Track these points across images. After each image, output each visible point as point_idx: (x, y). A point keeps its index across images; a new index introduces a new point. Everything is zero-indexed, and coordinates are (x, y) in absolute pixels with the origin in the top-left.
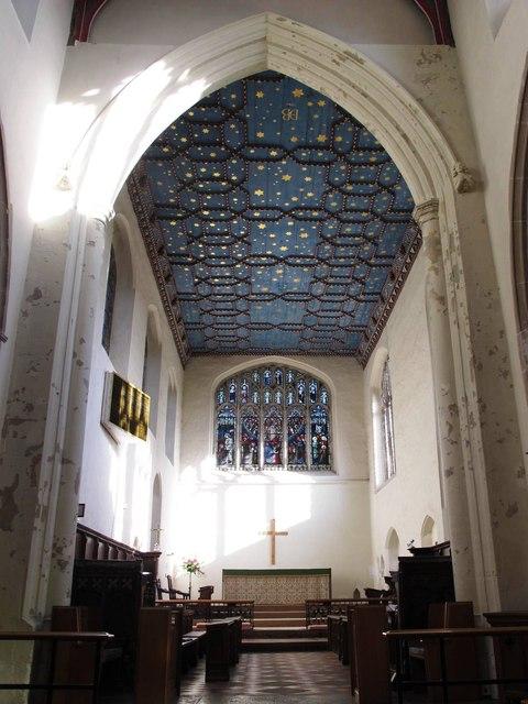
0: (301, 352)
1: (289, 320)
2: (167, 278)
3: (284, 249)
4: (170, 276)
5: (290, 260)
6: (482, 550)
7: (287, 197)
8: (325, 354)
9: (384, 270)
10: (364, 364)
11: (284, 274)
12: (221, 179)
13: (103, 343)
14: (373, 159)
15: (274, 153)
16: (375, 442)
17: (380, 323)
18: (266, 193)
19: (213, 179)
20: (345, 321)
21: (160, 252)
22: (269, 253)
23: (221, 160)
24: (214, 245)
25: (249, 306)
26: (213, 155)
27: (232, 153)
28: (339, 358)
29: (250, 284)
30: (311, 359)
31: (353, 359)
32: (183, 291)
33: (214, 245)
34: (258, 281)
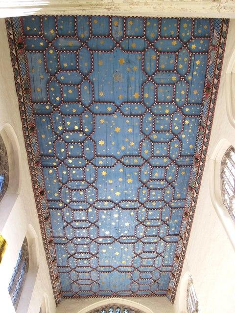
0: (134, 295)
1: (124, 263)
2: (46, 219)
3: (118, 194)
4: (48, 217)
5: (122, 204)
6: (229, 238)
7: (118, 147)
8: (147, 295)
9: (180, 211)
10: (172, 300)
11: (119, 218)
12: (80, 131)
13: (11, 290)
14: (167, 111)
15: (109, 109)
16: (38, 253)
17: (180, 258)
18: (106, 142)
19: (74, 131)
20: (158, 262)
21: (42, 193)
22: (109, 198)
23: (79, 114)
24: (75, 190)
25: (98, 248)
26: (74, 111)
27: (87, 108)
28: (157, 298)
29: (98, 227)
30: (139, 299)
31: (165, 298)
32: (57, 235)
33: (75, 190)
34: (104, 226)
